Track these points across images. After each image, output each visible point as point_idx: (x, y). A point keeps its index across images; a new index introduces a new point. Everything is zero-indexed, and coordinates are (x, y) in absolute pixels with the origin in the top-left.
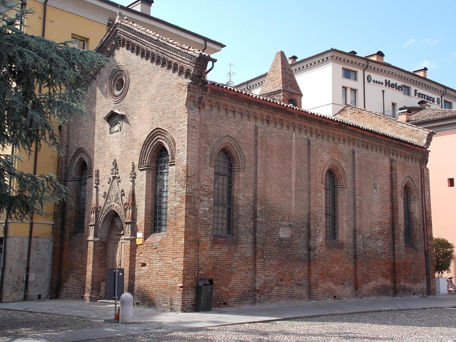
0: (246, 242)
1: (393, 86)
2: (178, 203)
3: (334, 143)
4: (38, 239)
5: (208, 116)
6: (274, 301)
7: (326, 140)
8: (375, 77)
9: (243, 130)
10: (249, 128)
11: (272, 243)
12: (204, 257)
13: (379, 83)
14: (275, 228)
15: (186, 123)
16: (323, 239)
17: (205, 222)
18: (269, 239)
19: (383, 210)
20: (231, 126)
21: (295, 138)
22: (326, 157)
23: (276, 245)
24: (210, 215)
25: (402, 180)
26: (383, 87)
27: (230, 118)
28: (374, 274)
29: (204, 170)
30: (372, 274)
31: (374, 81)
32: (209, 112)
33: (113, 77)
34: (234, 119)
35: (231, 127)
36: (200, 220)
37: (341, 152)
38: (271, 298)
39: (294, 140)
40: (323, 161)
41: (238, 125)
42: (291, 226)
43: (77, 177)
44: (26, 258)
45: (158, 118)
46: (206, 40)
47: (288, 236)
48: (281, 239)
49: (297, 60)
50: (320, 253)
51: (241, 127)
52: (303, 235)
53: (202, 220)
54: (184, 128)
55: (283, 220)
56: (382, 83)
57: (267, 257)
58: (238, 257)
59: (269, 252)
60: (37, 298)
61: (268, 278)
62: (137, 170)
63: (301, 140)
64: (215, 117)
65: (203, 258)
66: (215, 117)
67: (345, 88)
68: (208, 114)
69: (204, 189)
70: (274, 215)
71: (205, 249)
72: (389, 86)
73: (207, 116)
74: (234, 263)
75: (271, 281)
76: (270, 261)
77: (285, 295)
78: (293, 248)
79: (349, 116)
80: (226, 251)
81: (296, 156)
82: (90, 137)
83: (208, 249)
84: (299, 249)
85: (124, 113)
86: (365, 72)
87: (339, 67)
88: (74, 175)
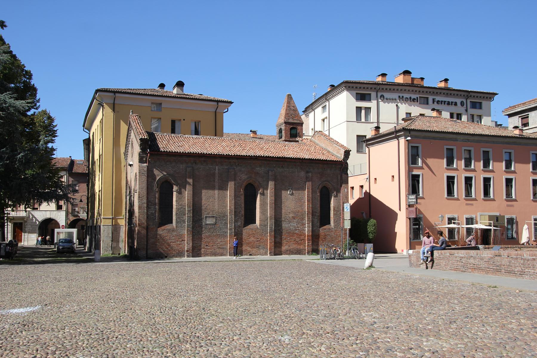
8: (386, 95)
13: (393, 99)
22: (244, 177)
30: (285, 242)
37: (258, 173)
39: (217, 170)
46: (218, 101)
50: (238, 231)
67: (359, 109)
71: (153, 231)
86: (378, 93)
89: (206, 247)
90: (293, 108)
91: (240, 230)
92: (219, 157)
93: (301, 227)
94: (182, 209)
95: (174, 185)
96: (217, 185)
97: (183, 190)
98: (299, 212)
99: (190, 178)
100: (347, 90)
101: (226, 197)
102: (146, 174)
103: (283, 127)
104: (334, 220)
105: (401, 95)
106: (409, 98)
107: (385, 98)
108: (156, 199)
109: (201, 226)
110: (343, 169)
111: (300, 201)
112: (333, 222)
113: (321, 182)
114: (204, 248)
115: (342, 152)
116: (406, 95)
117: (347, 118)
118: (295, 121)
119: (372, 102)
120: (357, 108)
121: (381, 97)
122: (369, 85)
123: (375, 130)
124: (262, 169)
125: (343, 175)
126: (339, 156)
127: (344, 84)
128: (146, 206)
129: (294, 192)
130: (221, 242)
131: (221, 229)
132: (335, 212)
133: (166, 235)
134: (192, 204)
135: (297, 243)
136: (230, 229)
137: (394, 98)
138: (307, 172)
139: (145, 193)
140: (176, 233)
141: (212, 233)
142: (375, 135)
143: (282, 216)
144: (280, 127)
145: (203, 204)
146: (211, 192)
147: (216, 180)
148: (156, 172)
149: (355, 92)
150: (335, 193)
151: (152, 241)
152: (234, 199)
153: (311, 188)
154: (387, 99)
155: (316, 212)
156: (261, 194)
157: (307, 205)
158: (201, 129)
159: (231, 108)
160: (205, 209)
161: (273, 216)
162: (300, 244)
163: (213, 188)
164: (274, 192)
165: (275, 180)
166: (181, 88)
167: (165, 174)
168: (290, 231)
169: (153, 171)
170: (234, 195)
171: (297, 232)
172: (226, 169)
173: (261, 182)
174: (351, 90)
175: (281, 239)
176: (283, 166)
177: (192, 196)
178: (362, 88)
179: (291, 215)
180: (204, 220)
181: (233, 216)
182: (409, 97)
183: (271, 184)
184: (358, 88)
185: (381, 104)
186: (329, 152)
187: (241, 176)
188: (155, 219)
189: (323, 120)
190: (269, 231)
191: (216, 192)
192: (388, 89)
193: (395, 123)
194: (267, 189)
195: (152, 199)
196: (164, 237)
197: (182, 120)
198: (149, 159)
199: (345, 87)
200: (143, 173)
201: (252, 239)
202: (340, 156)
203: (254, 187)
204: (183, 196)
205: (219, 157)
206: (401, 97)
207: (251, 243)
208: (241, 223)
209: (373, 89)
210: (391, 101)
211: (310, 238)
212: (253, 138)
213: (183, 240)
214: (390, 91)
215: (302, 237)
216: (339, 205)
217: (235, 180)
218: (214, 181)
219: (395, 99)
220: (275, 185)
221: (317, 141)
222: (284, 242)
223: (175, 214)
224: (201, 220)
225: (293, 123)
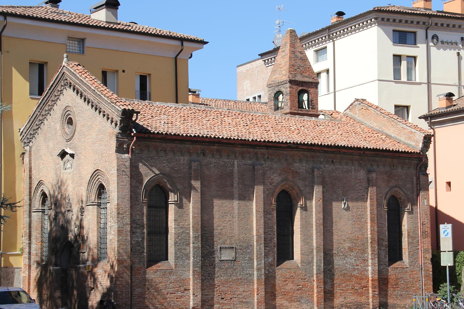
2: (113, 236)
3: (287, 164)
4: (7, 269)
5: (138, 158)
7: (276, 162)
8: (443, 35)
9: (176, 165)
10: (183, 163)
11: (211, 265)
12: (138, 280)
13: (452, 43)
15: (116, 168)
17: (138, 251)
18: (208, 262)
20: (163, 164)
21: (237, 165)
22: (276, 178)
25: (386, 191)
27: (161, 157)
28: (341, 291)
29: (136, 206)
30: (339, 291)
32: (139, 155)
33: (64, 116)
34: (166, 157)
35: (163, 165)
36: (134, 249)
37: (297, 172)
39: (236, 167)
40: (273, 183)
41: (171, 162)
43: (41, 208)
45: (98, 160)
46: (182, 40)
49: (345, 17)
50: (269, 272)
51: (174, 163)
53: (135, 249)
54: (115, 172)
57: (205, 278)
59: (208, 273)
61: (207, 296)
63: (245, 166)
64: (146, 159)
65: (137, 281)
66: (146, 159)
67: (398, 58)
68: (138, 157)
69: (136, 222)
71: (140, 273)
73: (137, 159)
75: (211, 299)
76: (210, 281)
78: (236, 269)
79: (357, 112)
81: (238, 182)
82: (49, 171)
83: (142, 273)
85: (74, 153)
86: (428, 31)
88: (38, 206)
89: (221, 302)
90: (301, 56)
91: (271, 271)
92: (240, 144)
93: (362, 265)
94: (184, 234)
95: (172, 192)
96: (236, 191)
97: (185, 200)
98: (357, 240)
99: (196, 179)
100: (379, 25)
101: (249, 213)
102: (128, 173)
104: (409, 252)
107: (440, 40)
108: (143, 217)
109: (213, 265)
110: (420, 167)
111: (360, 219)
112: (407, 256)
113: (388, 189)
114: (218, 303)
115: (420, 138)
117: (379, 74)
118: (306, 80)
119: (418, 47)
121: (433, 38)
122: (414, 17)
123: (447, 99)
124: (303, 166)
125: (421, 176)
126: (413, 144)
127: (374, 14)
128: (129, 229)
129: (350, 204)
130: (244, 291)
131: (243, 270)
132: (410, 240)
133: (160, 280)
134: (200, 226)
135: (356, 292)
136: (258, 269)
137: (454, 41)
138: (369, 172)
139: (128, 206)
140: (174, 277)
141: (231, 276)
142: (447, 107)
143: (333, 245)
145: (215, 225)
146: (226, 203)
147: (235, 185)
148: (143, 169)
149: (391, 29)
150: (409, 206)
151: (138, 291)
152: (263, 217)
153: (375, 199)
154: (442, 42)
155: (383, 240)
156: (302, 208)
157: (371, 227)
158: (151, 86)
160: (220, 234)
161: (322, 247)
162: (361, 294)
163: (230, 197)
164: (322, 205)
165: (323, 183)
166: (115, 10)
167: (157, 172)
168: (345, 271)
169: (137, 168)
170: (263, 210)
171: (355, 273)
172: (250, 165)
173: (302, 188)
174: (385, 25)
175: (333, 285)
176: (334, 161)
177: (200, 210)
178: (403, 22)
179: (347, 245)
180: (217, 254)
181: (262, 246)
183: (318, 191)
184: (397, 21)
185: (433, 50)
187: (272, 177)
188: (143, 252)
190: (315, 272)
191: (236, 203)
192: (445, 25)
193: (456, 85)
194: (311, 199)
195: (138, 217)
196: (156, 285)
197: (120, 72)
198: (133, 145)
199: (376, 19)
200: (123, 171)
201: (290, 286)
202: (417, 146)
203: (290, 197)
204: (185, 212)
205: (240, 144)
207: (288, 293)
208: (274, 259)
209: (421, 23)
210: (450, 45)
211: (376, 284)
212: (193, 103)
213: (185, 290)
214: (448, 28)
215: (364, 283)
216: (415, 227)
217: (264, 184)
218: (232, 185)
219: (456, 44)
220: (323, 192)
221: (358, 117)
222: (337, 291)
223: (173, 243)
224: (212, 253)
225: (302, 82)
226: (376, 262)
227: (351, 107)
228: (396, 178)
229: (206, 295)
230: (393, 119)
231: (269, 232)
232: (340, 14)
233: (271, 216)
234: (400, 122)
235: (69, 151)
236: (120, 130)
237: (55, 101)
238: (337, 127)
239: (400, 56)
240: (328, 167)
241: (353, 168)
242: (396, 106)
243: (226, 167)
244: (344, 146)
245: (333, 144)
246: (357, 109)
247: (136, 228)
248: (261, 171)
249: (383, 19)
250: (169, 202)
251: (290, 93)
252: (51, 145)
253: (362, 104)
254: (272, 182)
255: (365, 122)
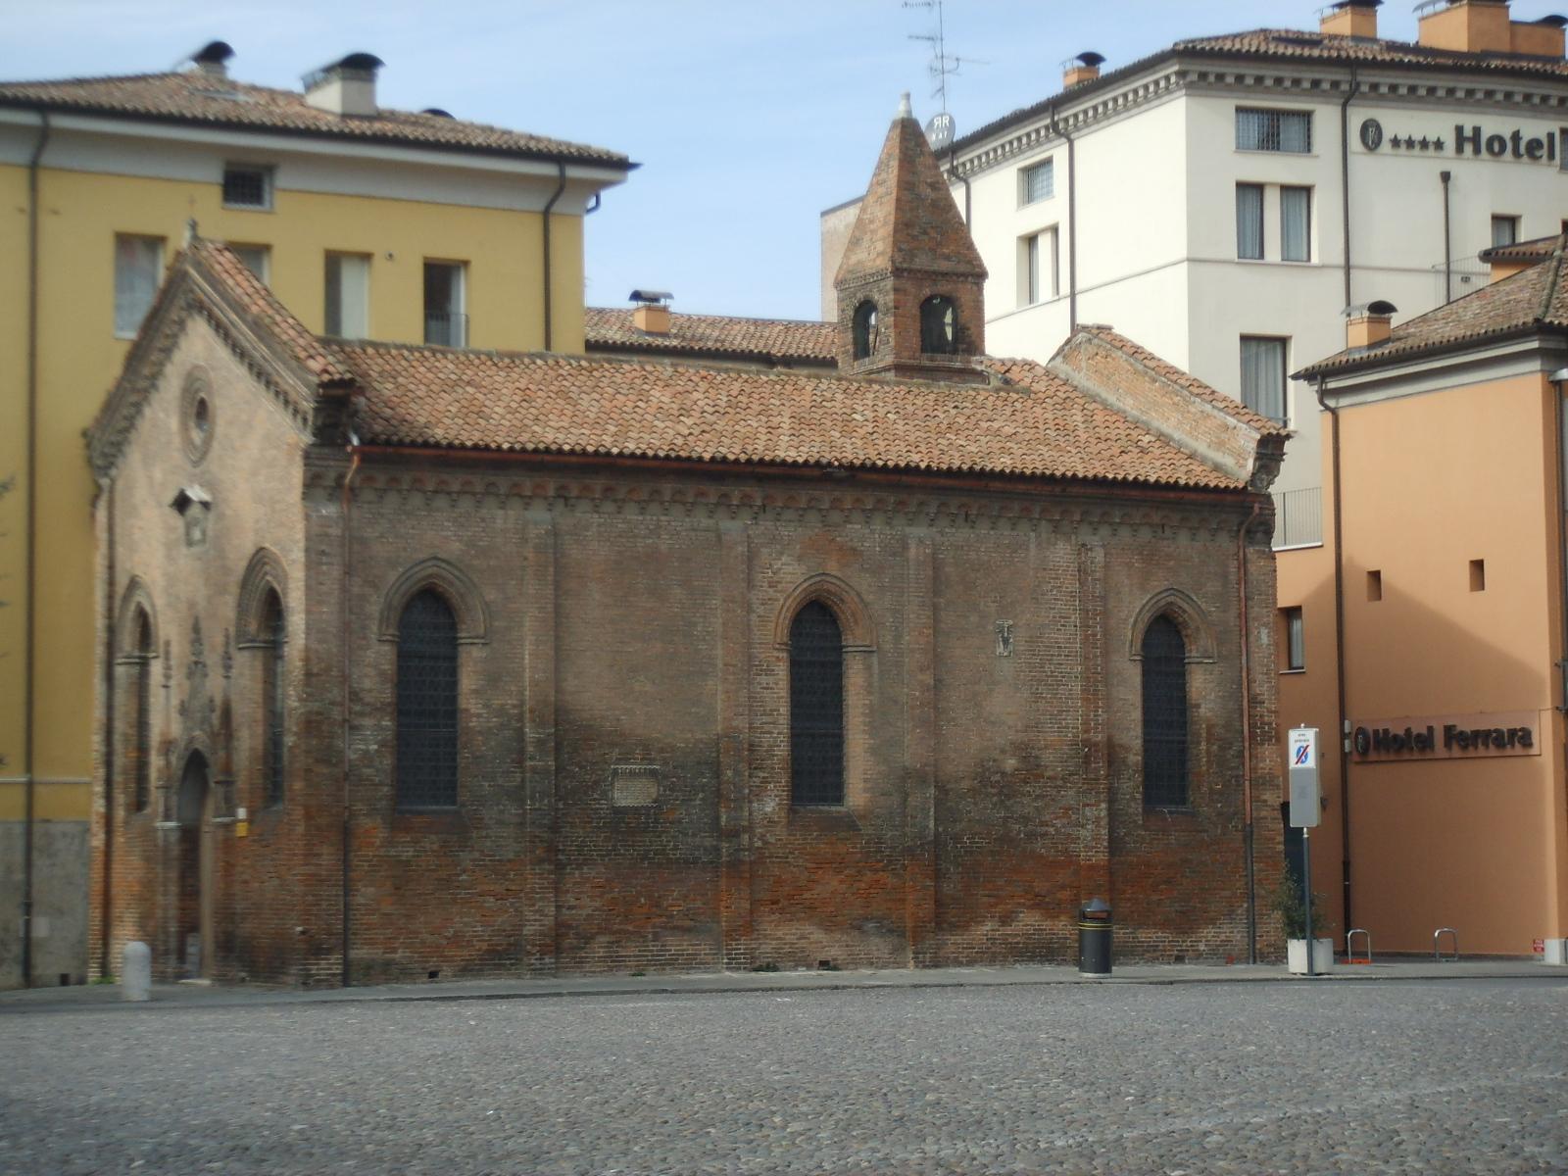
0: (500, 823)
1: (1496, 146)
6: (594, 972)
8: (1397, 122)
14: (596, 783)
15: (302, 544)
16: (779, 804)
19: (1042, 705)
22: (790, 569)
23: (599, 828)
24: (381, 762)
26: (1448, 160)
28: (992, 900)
30: (985, 899)
31: (1395, 142)
37: (854, 549)
38: (582, 962)
42: (653, 773)
44: (19, 876)
47: (648, 802)
48: (619, 812)
49: (1104, 69)
50: (766, 843)
52: (701, 796)
55: (625, 759)
56: (1439, 145)
58: (471, 860)
60: (57, 980)
62: (233, 651)
63: (693, 534)
67: (1250, 191)
70: (592, 750)
72: (1477, 151)
74: (459, 875)
77: (635, 956)
78: (664, 832)
79: (1084, 364)
80: (435, 847)
84: (686, 835)
87: (1220, 115)
103: (884, 297)
105: (1469, 121)
106: (1507, 136)
115: (1247, 440)
116: (1494, 125)
118: (944, 266)
120: (1243, 187)
123: (1371, 320)
124: (872, 532)
126: (1228, 461)
137: (1432, 138)
142: (1371, 346)
144: (860, 296)
159: (632, 175)
173: (869, 598)
182: (1507, 135)
186: (1163, 439)
189: (1031, 240)
197: (379, 262)
199: (1181, 74)
206: (1468, 132)
226: (1103, 814)
227: (1067, 348)
228: (1172, 563)
229: (570, 908)
230: (1177, 387)
231: (766, 728)
232: (1092, 59)
233: (771, 679)
234: (1197, 395)
235: (196, 493)
236: (315, 435)
237: (167, 351)
238: (1009, 410)
239: (1258, 188)
240: (953, 535)
241: (1033, 534)
242: (1245, 339)
243: (635, 536)
244: (1002, 471)
245: (965, 467)
246: (1082, 357)
247: (362, 714)
248: (740, 549)
249: (1203, 76)
250: (463, 641)
251: (896, 308)
252: (158, 475)
253: (1096, 341)
254: (775, 579)
255: (1104, 395)
